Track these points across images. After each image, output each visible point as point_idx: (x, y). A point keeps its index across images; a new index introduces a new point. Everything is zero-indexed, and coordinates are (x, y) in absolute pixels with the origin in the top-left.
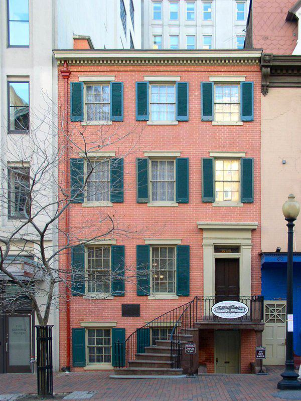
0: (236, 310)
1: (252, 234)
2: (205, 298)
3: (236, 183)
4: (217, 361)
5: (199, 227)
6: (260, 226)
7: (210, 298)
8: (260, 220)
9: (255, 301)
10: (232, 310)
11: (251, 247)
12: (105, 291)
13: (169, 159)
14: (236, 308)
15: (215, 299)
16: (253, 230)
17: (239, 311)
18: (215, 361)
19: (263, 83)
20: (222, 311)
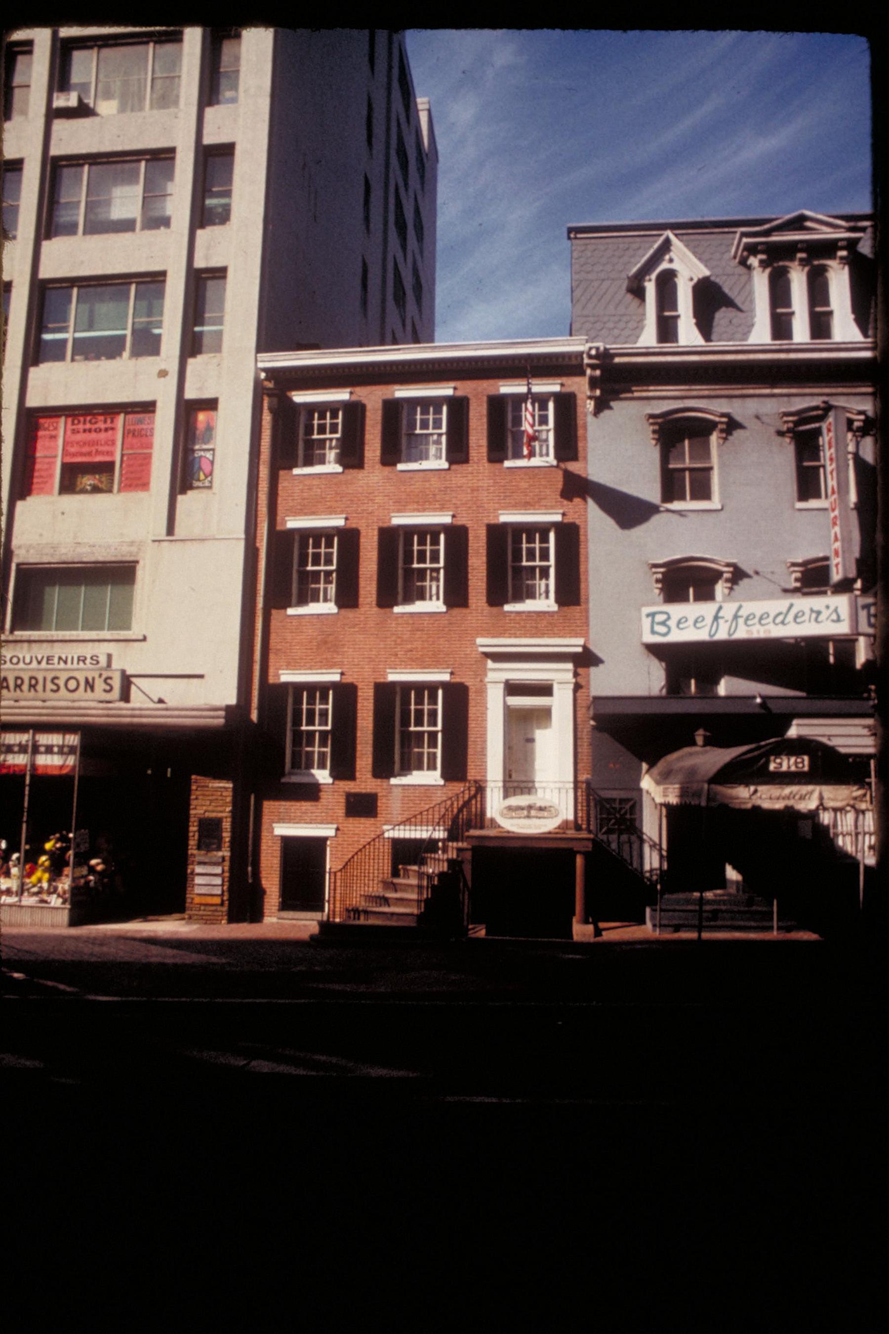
11: (571, 686)
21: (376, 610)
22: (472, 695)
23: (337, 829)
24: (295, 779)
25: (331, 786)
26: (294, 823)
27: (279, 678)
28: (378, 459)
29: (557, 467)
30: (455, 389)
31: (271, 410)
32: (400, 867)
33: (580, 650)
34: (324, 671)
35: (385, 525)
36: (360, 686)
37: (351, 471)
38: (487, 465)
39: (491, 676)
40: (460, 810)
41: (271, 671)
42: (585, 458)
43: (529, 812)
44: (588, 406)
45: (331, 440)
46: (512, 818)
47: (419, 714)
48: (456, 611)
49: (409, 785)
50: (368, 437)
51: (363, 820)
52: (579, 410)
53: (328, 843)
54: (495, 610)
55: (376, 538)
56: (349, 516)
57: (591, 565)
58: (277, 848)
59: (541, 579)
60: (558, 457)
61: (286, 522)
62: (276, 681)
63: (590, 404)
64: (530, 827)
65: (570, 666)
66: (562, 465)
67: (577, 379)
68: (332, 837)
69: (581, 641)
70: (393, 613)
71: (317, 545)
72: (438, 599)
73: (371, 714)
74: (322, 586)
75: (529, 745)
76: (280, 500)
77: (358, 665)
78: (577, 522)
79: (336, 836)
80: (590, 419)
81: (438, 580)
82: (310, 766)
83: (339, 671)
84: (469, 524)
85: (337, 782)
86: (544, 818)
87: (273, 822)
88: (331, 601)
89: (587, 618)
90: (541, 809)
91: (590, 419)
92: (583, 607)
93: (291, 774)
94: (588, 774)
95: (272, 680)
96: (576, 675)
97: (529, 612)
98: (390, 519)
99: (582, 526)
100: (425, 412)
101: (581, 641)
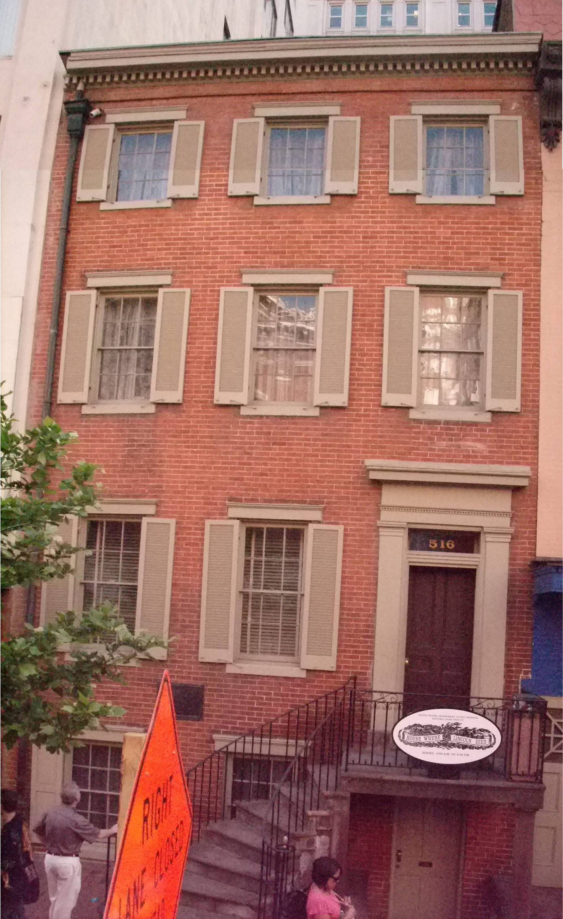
0: (465, 740)
1: (513, 496)
2: (376, 696)
3: (470, 356)
4: (399, 859)
5: (373, 476)
6: (534, 479)
7: (388, 698)
8: (534, 465)
9: (521, 713)
10: (454, 738)
11: (508, 539)
12: (466, 194)
13: (146, 292)
14: (466, 732)
15: (404, 703)
16: (516, 490)
17: (473, 741)
18: (394, 857)
19: (546, 117)
20: (422, 739)
89: (537, 437)
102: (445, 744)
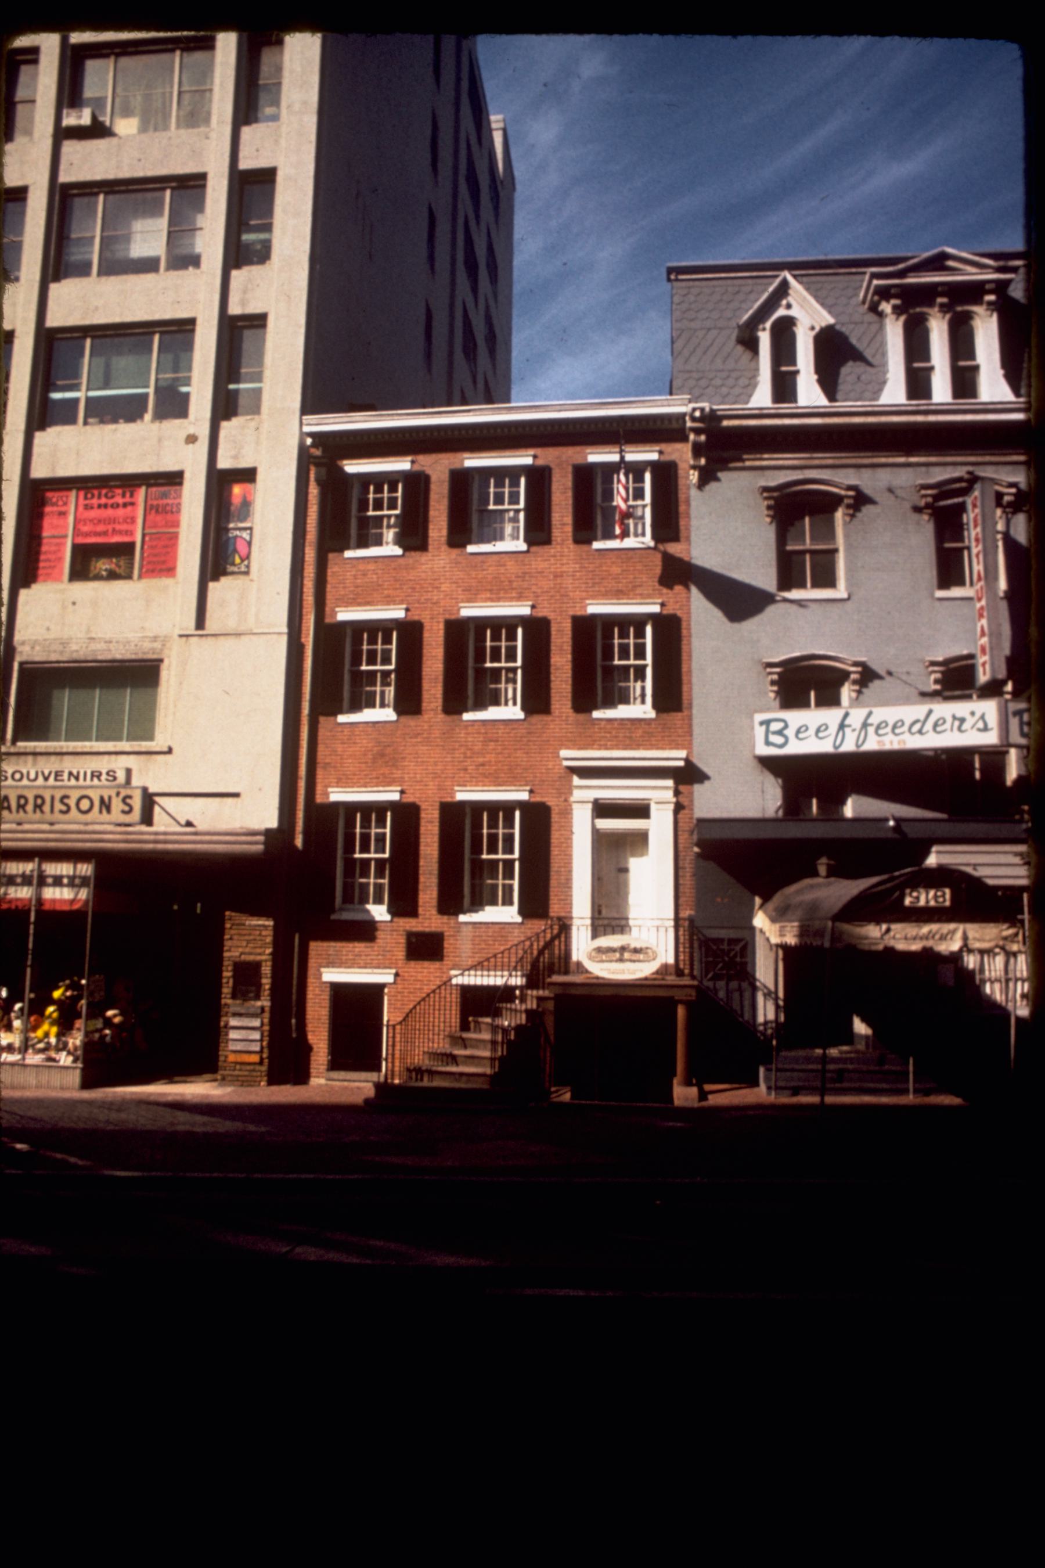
11: (672, 807)
21: (441, 717)
22: (555, 817)
23: (397, 975)
24: (346, 916)
25: (389, 924)
26: (346, 967)
27: (328, 798)
28: (444, 539)
29: (655, 548)
30: (535, 457)
31: (318, 481)
32: (471, 1019)
33: (681, 763)
34: (381, 789)
35: (453, 617)
36: (423, 806)
37: (413, 554)
38: (572, 546)
39: (577, 795)
40: (541, 952)
41: (319, 788)
42: (688, 539)
43: (622, 955)
44: (691, 477)
45: (389, 517)
46: (602, 961)
47: (493, 839)
48: (536, 719)
49: (481, 923)
50: (432, 513)
51: (426, 964)
52: (681, 482)
53: (386, 990)
54: (582, 717)
55: (442, 633)
56: (410, 606)
57: (695, 665)
58: (326, 997)
59: (636, 681)
60: (654, 537)
61: (336, 613)
62: (325, 801)
63: (694, 475)
64: (623, 972)
65: (670, 783)
66: (661, 547)
67: (679, 446)
68: (390, 984)
69: (683, 754)
70: (461, 720)
71: (372, 641)
72: (515, 704)
73: (436, 839)
74: (378, 689)
75: (622, 875)
76: (329, 588)
77: (421, 781)
78: (679, 613)
79: (395, 983)
80: (694, 492)
81: (515, 682)
82: (364, 900)
83: (399, 788)
84: (551, 616)
85: (396, 920)
86: (639, 961)
87: (321, 966)
88: (388, 706)
89: (690, 726)
90: (636, 951)
91: (694, 492)
92: (686, 713)
93: (341, 909)
94: (691, 909)
95: (319, 799)
96: (677, 793)
97: (622, 720)
98: (458, 610)
99: (684, 617)
100: (499, 484)
101: (683, 754)
102: (621, 960)
